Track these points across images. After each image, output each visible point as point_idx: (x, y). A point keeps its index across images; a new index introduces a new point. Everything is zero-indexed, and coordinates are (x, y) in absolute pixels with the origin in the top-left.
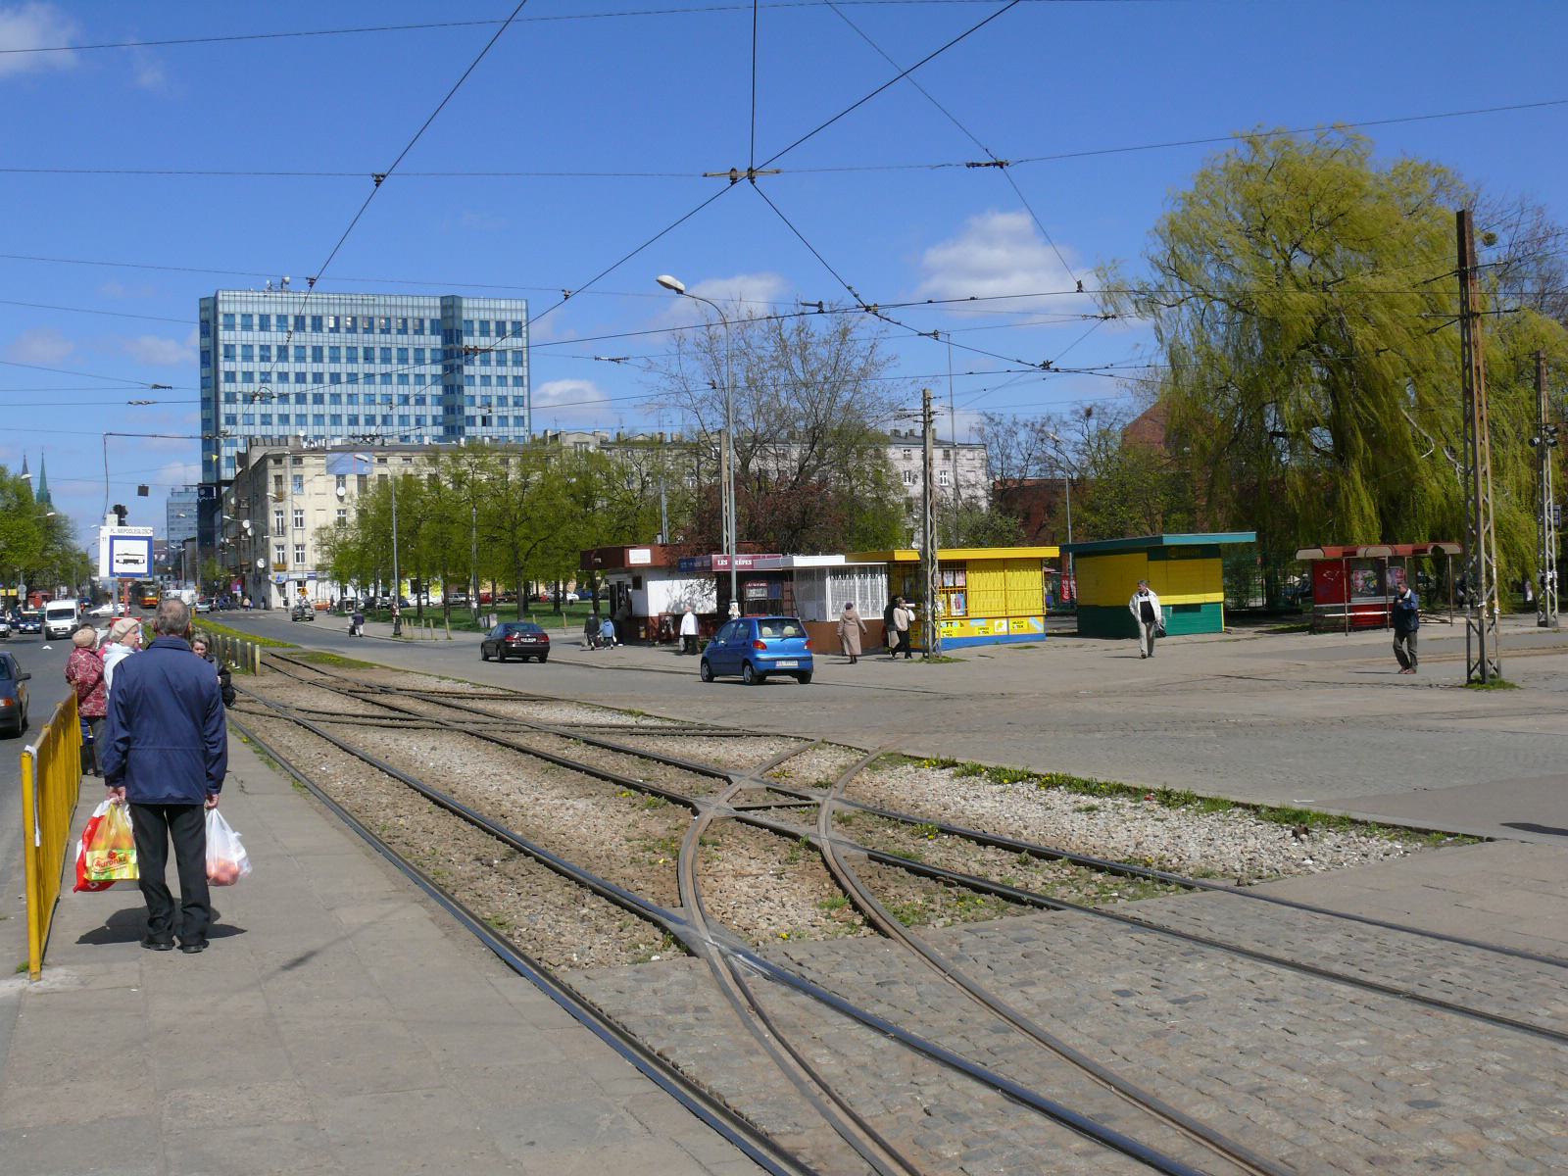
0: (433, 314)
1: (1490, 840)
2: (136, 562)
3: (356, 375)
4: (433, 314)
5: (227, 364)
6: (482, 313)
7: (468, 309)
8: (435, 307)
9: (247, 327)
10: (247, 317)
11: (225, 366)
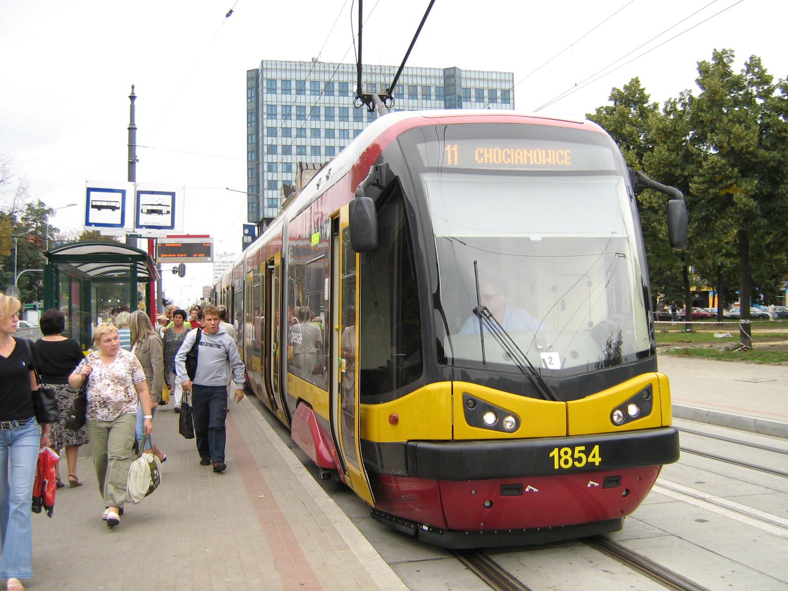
0: (438, 83)
1: (320, 179)
2: (159, 212)
3: (297, 119)
4: (438, 83)
5: (269, 121)
6: (477, 82)
7: (466, 79)
8: (439, 77)
9: (286, 90)
10: (286, 82)
11: (268, 123)
